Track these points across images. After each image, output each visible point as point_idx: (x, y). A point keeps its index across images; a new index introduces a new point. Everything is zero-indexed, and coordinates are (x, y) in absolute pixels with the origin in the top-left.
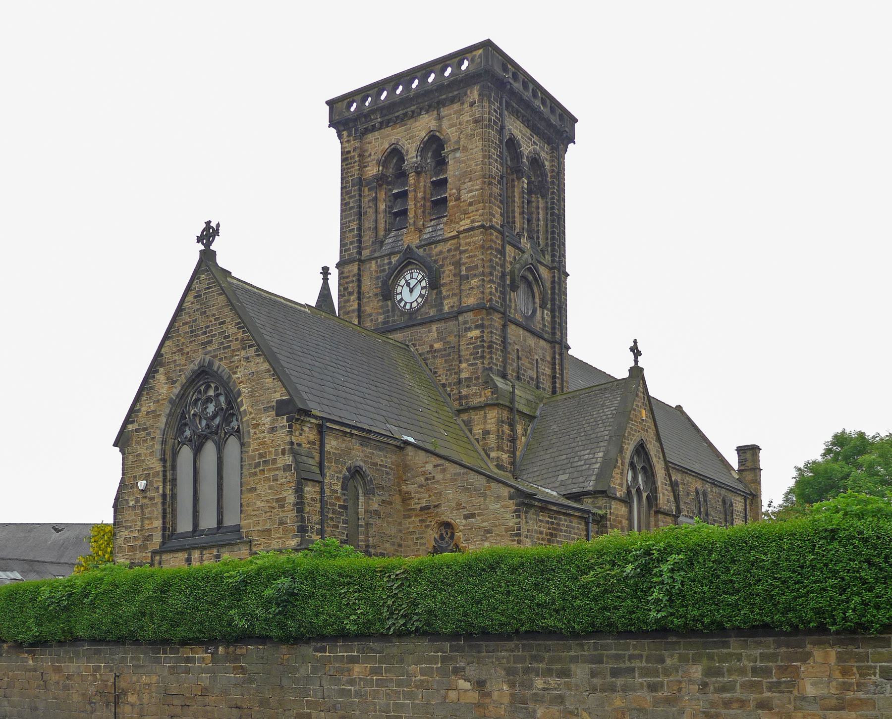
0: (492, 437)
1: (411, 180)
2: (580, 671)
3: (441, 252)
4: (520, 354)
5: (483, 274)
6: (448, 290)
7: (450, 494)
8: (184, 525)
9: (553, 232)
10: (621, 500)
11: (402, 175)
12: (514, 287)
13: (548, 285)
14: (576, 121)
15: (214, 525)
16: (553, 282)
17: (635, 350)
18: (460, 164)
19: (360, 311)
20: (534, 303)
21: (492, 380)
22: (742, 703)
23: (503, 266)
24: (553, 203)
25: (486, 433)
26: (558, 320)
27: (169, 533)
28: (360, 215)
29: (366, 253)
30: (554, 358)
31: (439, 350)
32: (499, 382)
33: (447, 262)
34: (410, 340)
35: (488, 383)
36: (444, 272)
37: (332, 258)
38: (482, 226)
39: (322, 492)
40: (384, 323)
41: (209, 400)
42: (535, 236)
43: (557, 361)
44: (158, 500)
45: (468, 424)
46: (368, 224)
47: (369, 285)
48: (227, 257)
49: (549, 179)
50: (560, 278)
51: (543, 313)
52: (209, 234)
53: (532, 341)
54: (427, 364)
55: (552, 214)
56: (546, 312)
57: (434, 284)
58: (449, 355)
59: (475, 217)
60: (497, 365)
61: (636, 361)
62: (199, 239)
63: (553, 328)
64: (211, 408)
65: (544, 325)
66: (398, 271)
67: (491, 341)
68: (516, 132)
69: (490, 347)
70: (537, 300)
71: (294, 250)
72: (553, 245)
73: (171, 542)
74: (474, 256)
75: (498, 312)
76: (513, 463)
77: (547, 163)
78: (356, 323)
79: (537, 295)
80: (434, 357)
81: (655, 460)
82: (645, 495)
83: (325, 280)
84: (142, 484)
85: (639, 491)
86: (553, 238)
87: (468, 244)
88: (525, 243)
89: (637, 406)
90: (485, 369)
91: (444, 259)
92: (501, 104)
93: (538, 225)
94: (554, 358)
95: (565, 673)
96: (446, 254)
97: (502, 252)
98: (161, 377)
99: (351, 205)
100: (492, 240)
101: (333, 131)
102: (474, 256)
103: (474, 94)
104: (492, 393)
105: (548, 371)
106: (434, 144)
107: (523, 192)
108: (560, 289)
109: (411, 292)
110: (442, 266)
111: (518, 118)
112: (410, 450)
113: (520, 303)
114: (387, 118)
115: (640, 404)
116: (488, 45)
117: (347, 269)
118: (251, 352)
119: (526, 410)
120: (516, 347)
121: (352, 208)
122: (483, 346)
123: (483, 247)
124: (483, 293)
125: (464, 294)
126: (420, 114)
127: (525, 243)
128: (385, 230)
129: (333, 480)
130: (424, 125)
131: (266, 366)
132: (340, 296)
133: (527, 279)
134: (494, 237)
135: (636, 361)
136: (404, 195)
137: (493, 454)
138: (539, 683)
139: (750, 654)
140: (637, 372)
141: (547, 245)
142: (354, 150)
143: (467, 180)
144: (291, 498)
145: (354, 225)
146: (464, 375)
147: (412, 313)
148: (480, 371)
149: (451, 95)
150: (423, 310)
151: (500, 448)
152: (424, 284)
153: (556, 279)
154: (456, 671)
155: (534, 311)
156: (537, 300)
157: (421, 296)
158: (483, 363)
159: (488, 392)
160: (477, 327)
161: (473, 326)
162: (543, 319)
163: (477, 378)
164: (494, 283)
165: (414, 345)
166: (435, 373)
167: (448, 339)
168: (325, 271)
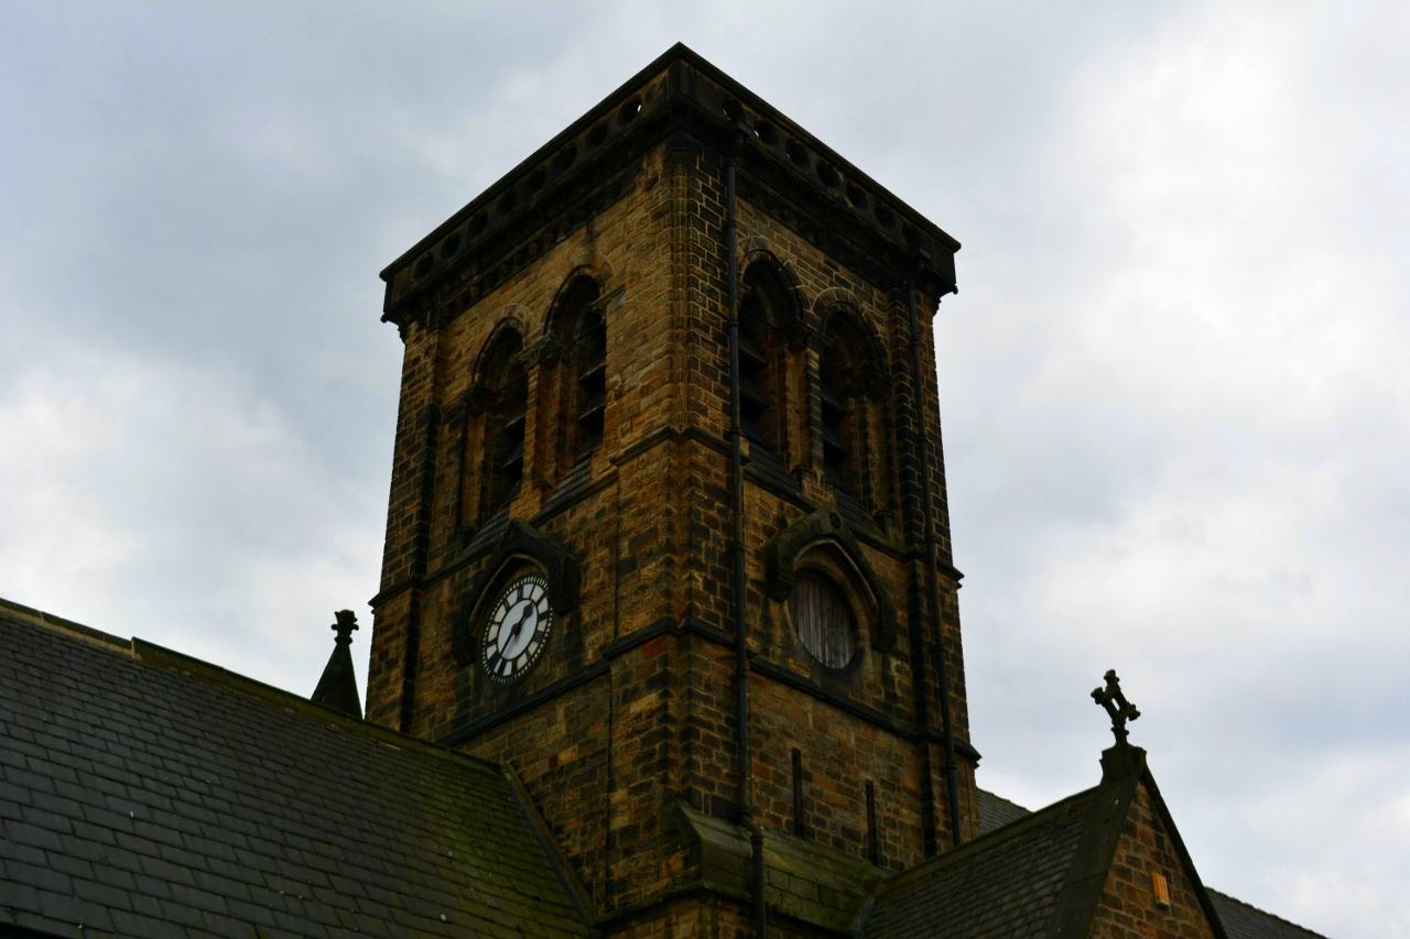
3: (583, 521)
4: (805, 763)
5: (669, 547)
6: (593, 610)
9: (906, 475)
12: (776, 585)
13: (896, 597)
14: (956, 246)
16: (913, 589)
17: (1110, 696)
20: (856, 638)
21: (686, 822)
24: (902, 410)
26: (932, 683)
29: (435, 565)
30: (926, 782)
31: (572, 766)
32: (712, 831)
33: (594, 542)
34: (508, 755)
36: (588, 566)
37: (360, 587)
38: (667, 434)
40: (457, 722)
42: (860, 487)
43: (936, 790)
46: (445, 500)
47: (434, 637)
49: (889, 361)
50: (931, 580)
51: (886, 665)
53: (846, 733)
54: (540, 810)
55: (902, 435)
56: (894, 663)
57: (564, 599)
58: (592, 773)
60: (711, 786)
61: (1120, 732)
63: (921, 704)
65: (891, 696)
67: (690, 719)
69: (687, 734)
70: (864, 631)
72: (908, 503)
74: (648, 509)
75: (714, 641)
77: (880, 328)
78: (397, 727)
79: (862, 618)
80: (558, 789)
83: (343, 642)
86: (907, 488)
87: (638, 484)
89: (1133, 861)
90: (671, 797)
91: (591, 534)
92: (725, 180)
93: (866, 463)
94: (926, 782)
96: (593, 525)
97: (730, 497)
99: (412, 465)
100: (693, 465)
102: (648, 509)
104: (687, 861)
105: (909, 817)
107: (808, 378)
108: (933, 607)
109: (517, 629)
110: (584, 554)
111: (784, 221)
114: (490, 269)
115: (1143, 857)
120: (791, 744)
121: (413, 472)
122: (666, 734)
123: (668, 482)
124: (668, 594)
125: (625, 605)
126: (554, 243)
128: (482, 507)
132: (373, 674)
133: (816, 571)
134: (700, 459)
135: (1120, 732)
140: (1125, 764)
141: (891, 504)
142: (427, 353)
143: (639, 341)
145: (412, 510)
146: (620, 822)
147: (521, 679)
148: (657, 804)
149: (609, 182)
150: (540, 670)
152: (544, 607)
153: (922, 582)
155: (857, 658)
156: (864, 631)
157: (537, 637)
158: (665, 780)
159: (676, 862)
160: (652, 685)
161: (642, 684)
162: (887, 679)
163: (650, 825)
164: (701, 567)
165: (516, 765)
166: (560, 829)
167: (590, 734)
168: (346, 622)
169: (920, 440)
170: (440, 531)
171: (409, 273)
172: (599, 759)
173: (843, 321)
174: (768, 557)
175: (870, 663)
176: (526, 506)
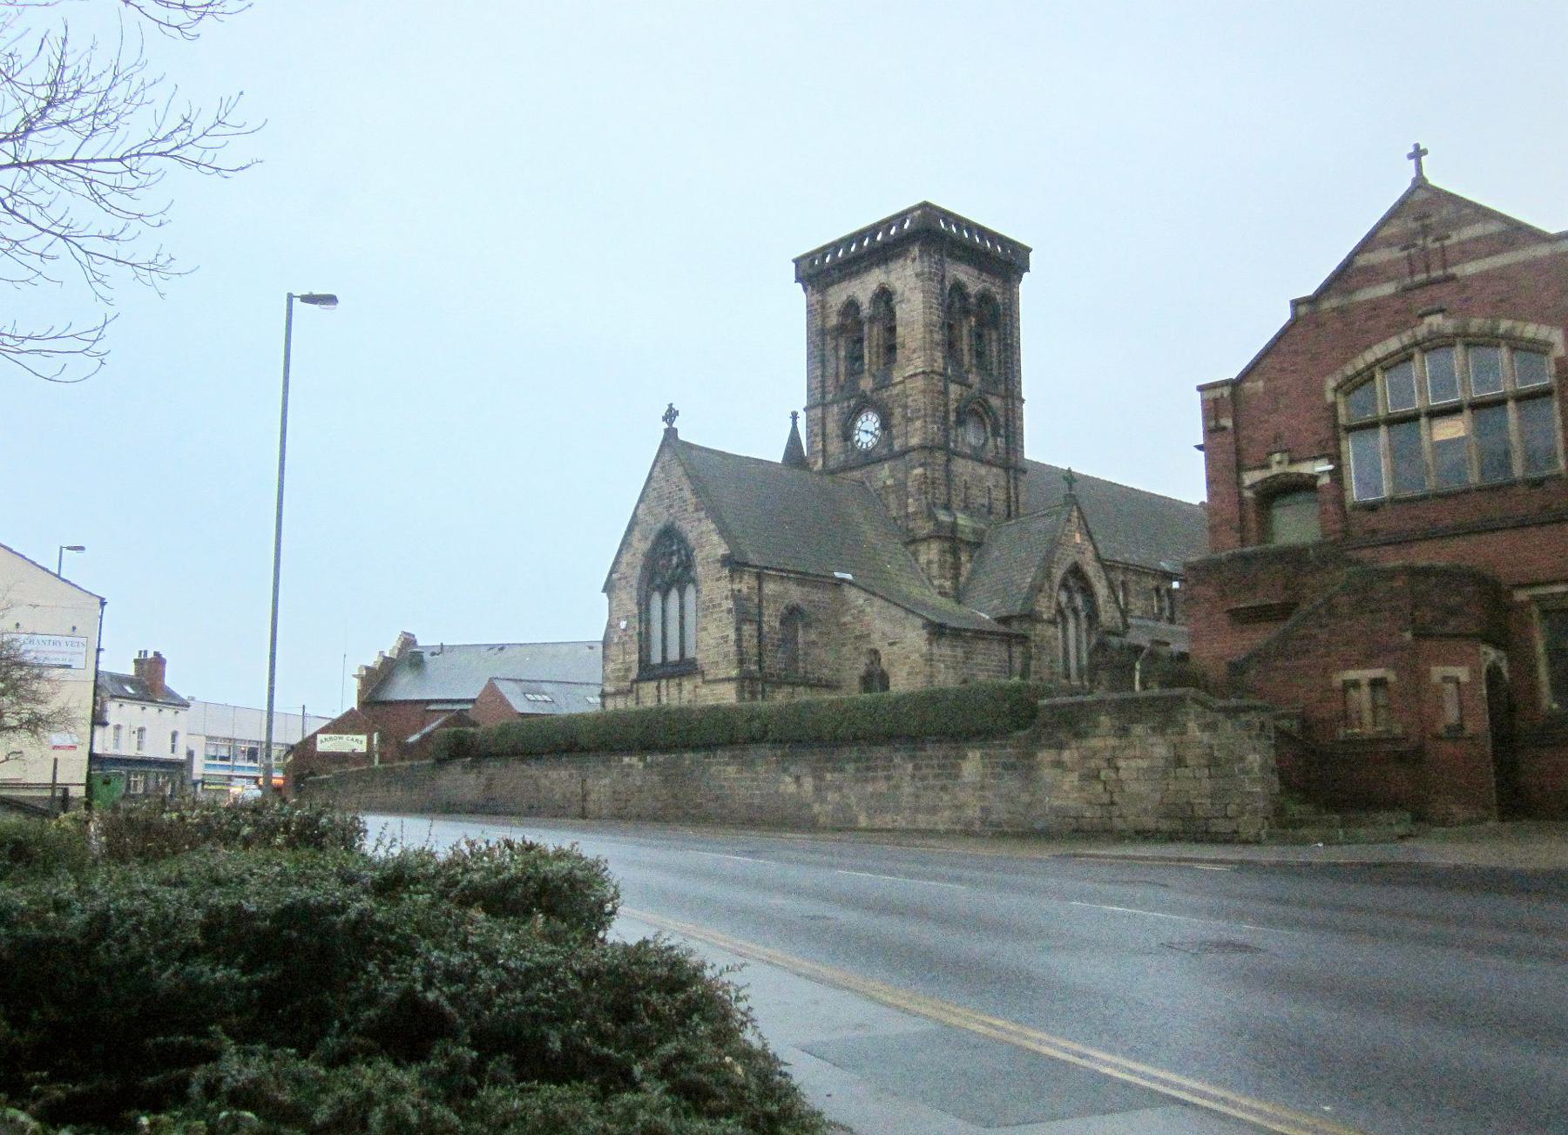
0: (935, 566)
1: (866, 328)
2: (850, 768)
7: (878, 624)
8: (656, 658)
10: (1053, 622)
11: (860, 324)
12: (960, 422)
13: (1001, 413)
15: (678, 658)
18: (381, 653)
19: (824, 450)
22: (933, 788)
23: (946, 405)
25: (930, 562)
27: (644, 663)
28: (823, 363)
29: (829, 397)
32: (943, 517)
35: (931, 516)
37: (800, 401)
39: (760, 629)
41: (672, 554)
44: (636, 638)
45: (915, 554)
46: (831, 370)
47: (832, 428)
48: (687, 432)
52: (671, 415)
53: (983, 471)
57: (885, 425)
59: (918, 364)
62: (665, 419)
64: (675, 560)
66: (856, 413)
68: (963, 277)
71: (760, 402)
73: (648, 672)
76: (956, 588)
81: (1094, 580)
82: (1083, 614)
83: (795, 424)
84: (623, 624)
85: (1075, 611)
88: (973, 378)
95: (842, 770)
98: (637, 534)
101: (799, 285)
103: (915, 251)
106: (885, 296)
109: (867, 429)
112: (846, 587)
113: (971, 436)
116: (925, 206)
117: (812, 413)
118: (702, 514)
119: (971, 538)
127: (973, 378)
129: (771, 621)
130: (873, 279)
131: (713, 526)
133: (973, 411)
135: (1070, 488)
136: (861, 340)
137: (936, 582)
138: (828, 776)
139: (934, 753)
144: (733, 636)
145: (819, 372)
146: (911, 510)
147: (867, 453)
151: (943, 576)
154: (785, 770)
155: (986, 440)
168: (795, 416)
169: (1011, 345)
170: (830, 382)
171: (806, 263)
172: (901, 487)
173: (985, 298)
174: (958, 412)
175: (991, 442)
176: (866, 384)
